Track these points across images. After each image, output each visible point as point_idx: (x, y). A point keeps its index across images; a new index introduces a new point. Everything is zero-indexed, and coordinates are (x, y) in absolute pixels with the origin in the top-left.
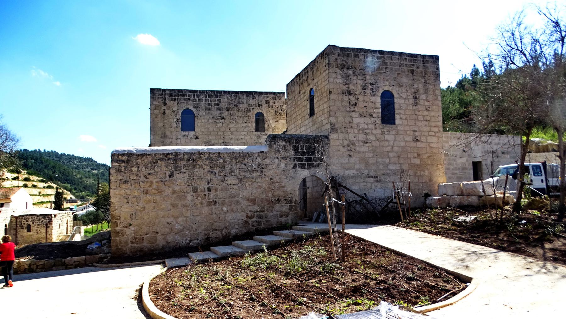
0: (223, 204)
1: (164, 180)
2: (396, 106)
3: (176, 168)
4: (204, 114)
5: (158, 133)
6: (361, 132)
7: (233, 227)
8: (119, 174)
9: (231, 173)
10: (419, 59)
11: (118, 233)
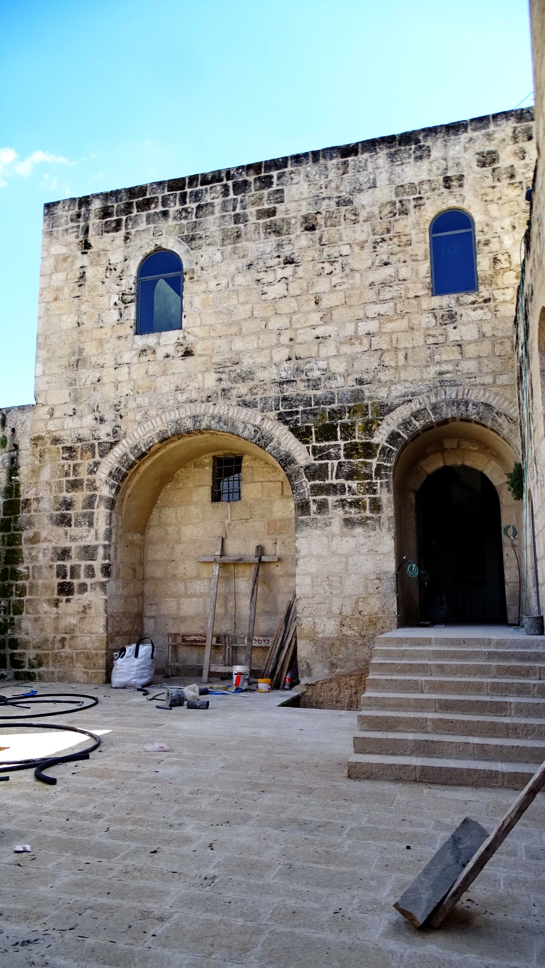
4: (218, 257)
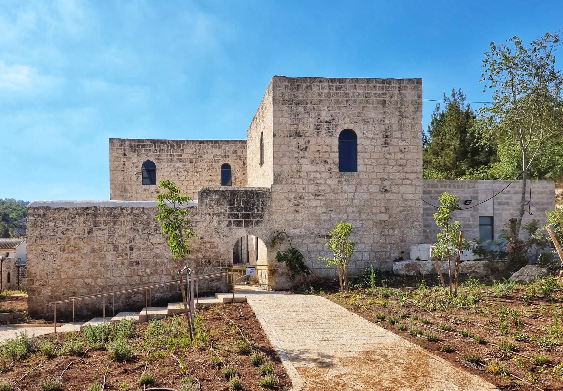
0: (147, 265)
1: (82, 237)
2: (359, 148)
3: (96, 224)
4: (166, 166)
5: (119, 188)
6: (312, 182)
7: (156, 292)
8: (35, 229)
9: (156, 230)
10: (394, 85)
11: (34, 291)
